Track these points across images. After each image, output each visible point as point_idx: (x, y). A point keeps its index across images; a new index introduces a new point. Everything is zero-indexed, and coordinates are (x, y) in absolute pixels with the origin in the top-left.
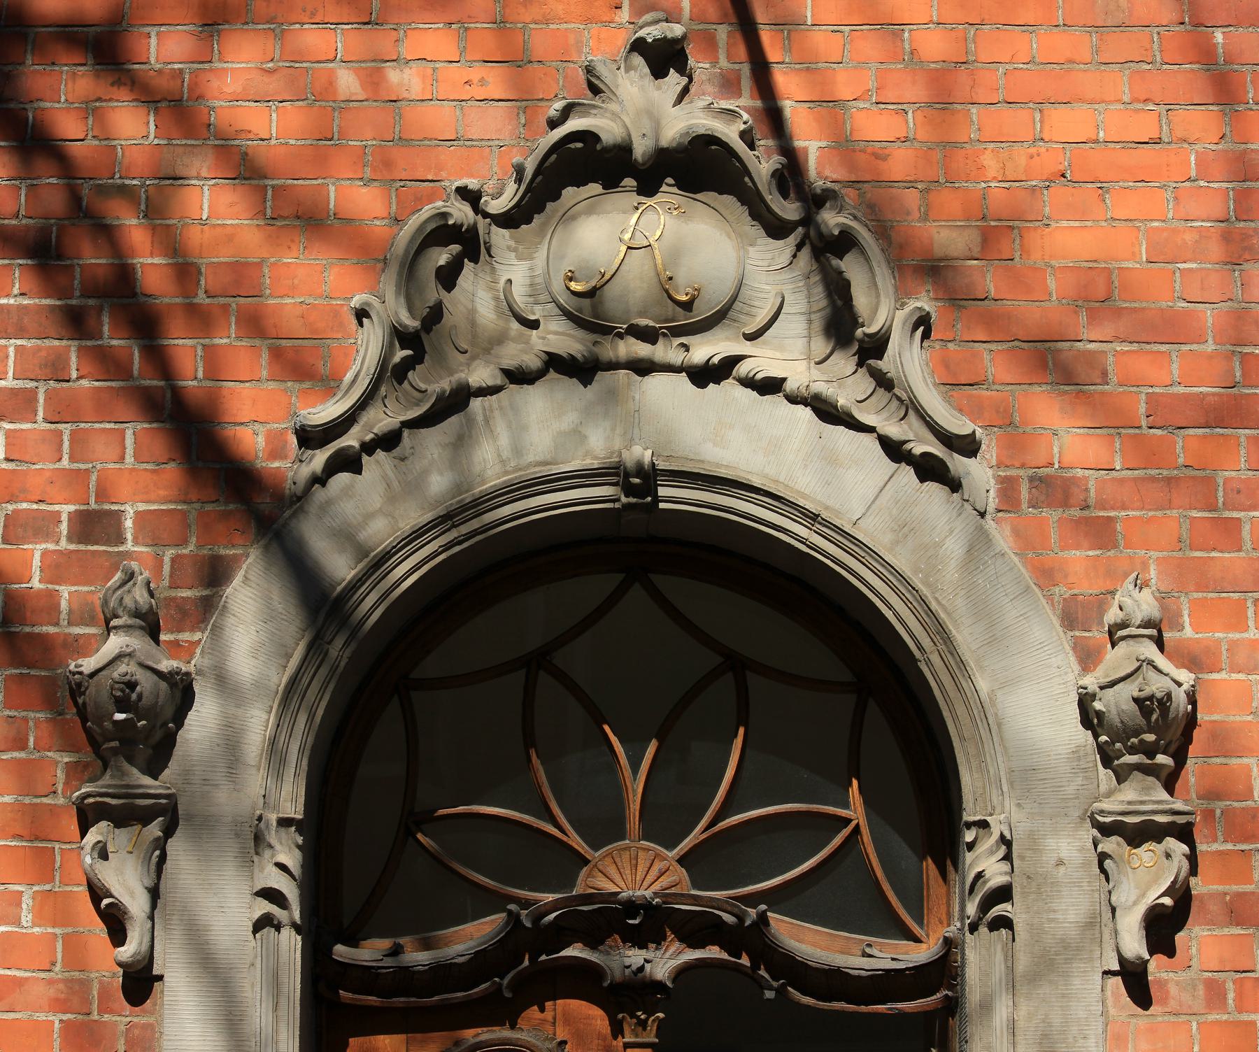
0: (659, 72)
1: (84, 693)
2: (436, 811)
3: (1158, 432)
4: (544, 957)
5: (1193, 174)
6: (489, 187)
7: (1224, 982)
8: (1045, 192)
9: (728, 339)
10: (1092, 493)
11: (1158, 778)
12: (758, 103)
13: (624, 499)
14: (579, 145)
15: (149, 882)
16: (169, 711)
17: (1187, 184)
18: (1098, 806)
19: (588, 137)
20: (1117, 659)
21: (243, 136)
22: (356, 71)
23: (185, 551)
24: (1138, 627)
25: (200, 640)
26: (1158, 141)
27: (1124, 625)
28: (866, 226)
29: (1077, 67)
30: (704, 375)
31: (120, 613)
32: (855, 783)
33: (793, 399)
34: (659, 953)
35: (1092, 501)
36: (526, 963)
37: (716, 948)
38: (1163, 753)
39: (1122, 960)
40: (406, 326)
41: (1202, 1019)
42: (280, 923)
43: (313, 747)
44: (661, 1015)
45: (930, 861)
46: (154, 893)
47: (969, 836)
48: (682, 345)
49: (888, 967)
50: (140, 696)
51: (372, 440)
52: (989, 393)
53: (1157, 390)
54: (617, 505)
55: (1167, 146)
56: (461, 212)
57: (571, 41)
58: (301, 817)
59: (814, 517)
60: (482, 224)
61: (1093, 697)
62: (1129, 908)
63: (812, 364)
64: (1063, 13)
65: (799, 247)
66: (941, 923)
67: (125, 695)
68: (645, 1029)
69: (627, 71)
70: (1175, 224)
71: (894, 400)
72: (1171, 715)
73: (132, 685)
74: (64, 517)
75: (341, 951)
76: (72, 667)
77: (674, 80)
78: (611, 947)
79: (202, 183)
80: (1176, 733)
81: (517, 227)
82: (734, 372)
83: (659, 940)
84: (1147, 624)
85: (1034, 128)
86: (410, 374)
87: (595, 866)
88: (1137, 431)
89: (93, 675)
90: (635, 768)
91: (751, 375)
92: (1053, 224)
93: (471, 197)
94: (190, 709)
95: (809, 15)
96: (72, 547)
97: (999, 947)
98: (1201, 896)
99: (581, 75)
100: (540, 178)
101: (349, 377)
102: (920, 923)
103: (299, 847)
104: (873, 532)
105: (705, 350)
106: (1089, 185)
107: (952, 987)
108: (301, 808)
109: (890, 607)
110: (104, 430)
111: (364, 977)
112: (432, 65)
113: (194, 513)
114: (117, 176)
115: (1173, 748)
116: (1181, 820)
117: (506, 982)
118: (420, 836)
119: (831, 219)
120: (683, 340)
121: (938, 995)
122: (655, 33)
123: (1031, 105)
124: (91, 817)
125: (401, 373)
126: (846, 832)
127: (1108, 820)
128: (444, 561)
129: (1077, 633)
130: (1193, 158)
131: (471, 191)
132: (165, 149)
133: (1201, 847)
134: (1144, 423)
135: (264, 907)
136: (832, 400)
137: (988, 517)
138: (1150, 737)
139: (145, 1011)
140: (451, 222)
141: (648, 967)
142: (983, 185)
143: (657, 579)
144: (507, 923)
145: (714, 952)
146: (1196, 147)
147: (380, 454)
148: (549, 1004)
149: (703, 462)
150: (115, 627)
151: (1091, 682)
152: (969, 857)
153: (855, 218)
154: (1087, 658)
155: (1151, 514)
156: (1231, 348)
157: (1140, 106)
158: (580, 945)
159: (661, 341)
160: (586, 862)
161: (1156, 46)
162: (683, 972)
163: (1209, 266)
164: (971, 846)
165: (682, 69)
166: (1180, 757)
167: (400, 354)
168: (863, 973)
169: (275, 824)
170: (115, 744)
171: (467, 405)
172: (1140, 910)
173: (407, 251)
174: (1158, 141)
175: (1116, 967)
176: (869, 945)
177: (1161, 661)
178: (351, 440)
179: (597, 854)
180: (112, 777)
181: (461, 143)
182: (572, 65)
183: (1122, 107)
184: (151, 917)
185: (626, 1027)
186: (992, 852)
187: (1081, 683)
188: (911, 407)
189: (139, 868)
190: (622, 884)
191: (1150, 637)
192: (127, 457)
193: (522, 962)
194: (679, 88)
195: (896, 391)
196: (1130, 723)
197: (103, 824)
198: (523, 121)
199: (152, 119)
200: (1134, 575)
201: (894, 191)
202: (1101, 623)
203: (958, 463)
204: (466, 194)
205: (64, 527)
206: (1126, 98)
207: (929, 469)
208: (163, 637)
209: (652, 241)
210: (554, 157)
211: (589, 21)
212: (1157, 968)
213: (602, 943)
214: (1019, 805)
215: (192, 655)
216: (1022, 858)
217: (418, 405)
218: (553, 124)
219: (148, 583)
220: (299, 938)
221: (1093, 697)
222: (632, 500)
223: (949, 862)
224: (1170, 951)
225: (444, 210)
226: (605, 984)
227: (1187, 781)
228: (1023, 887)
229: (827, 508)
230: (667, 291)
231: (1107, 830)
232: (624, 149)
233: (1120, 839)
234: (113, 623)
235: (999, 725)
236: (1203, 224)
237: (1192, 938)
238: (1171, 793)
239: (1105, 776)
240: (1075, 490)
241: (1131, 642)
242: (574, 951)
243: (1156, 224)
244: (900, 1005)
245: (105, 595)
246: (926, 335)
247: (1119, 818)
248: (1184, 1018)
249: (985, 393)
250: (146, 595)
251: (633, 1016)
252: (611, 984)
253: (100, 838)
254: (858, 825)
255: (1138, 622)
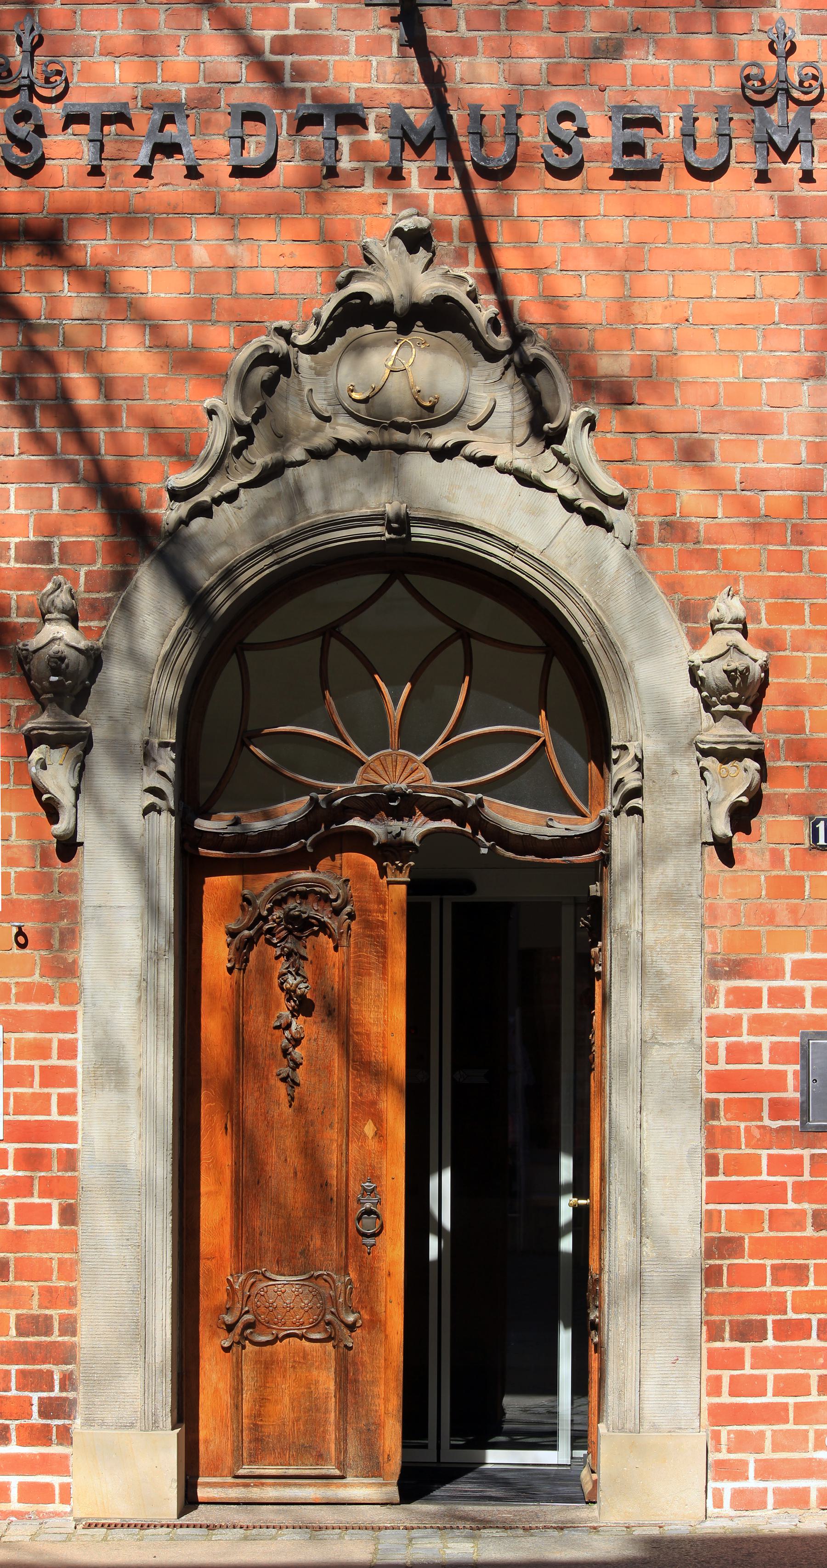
0: (412, 249)
1: (29, 663)
2: (263, 730)
3: (748, 493)
4: (334, 826)
5: (777, 319)
6: (298, 325)
7: (783, 850)
8: (675, 332)
9: (458, 430)
10: (702, 534)
11: (740, 720)
12: (482, 270)
13: (387, 536)
14: (358, 301)
15: (74, 783)
16: (85, 674)
17: (772, 326)
18: (700, 737)
19: (364, 296)
20: (716, 644)
21: (129, 290)
22: (206, 246)
23: (95, 568)
24: (730, 623)
25: (105, 627)
26: (753, 297)
27: (720, 621)
28: (552, 354)
29: (699, 246)
30: (442, 454)
31: (52, 610)
32: (543, 713)
33: (502, 470)
34: (411, 824)
35: (701, 539)
36: (323, 829)
37: (449, 821)
38: (744, 704)
39: (714, 836)
40: (241, 421)
41: (768, 874)
42: (160, 808)
43: (182, 696)
44: (412, 863)
45: (593, 764)
46: (77, 790)
47: (615, 755)
48: (427, 434)
49: (562, 834)
50: (67, 666)
51: (220, 496)
52: (634, 467)
53: (748, 465)
54: (383, 538)
55: (759, 301)
56: (278, 345)
57: (353, 226)
58: (174, 741)
59: (515, 548)
60: (293, 351)
61: (698, 667)
62: (720, 803)
63: (514, 446)
64: (691, 209)
65: (506, 368)
66: (600, 805)
67: (57, 663)
68: (401, 872)
69: (390, 249)
70: (763, 353)
71: (569, 471)
72: (749, 681)
73: (62, 659)
74: (13, 546)
75: (203, 825)
76: (20, 645)
77: (423, 255)
78: (378, 820)
79: (101, 323)
80: (753, 692)
81: (316, 353)
82: (462, 452)
83: (411, 815)
84: (735, 621)
85: (668, 288)
86: (244, 452)
87: (369, 766)
88: (734, 493)
89: (35, 651)
90: (395, 702)
91: (473, 454)
92: (680, 354)
93: (285, 334)
94: (100, 671)
95: (515, 209)
96: (18, 565)
97: (633, 826)
98: (769, 795)
99: (360, 251)
100: (331, 322)
101: (203, 453)
102: (586, 804)
103: (173, 760)
104: (557, 559)
105: (442, 438)
106: (705, 327)
107: (605, 848)
108: (174, 735)
109: (565, 606)
110: (38, 488)
111: (214, 840)
112: (257, 243)
113: (100, 543)
114: (43, 317)
115: (751, 701)
116: (754, 748)
117: (309, 842)
118: (252, 747)
119: (531, 350)
120: (428, 431)
121: (596, 853)
122: (410, 225)
123: (666, 272)
124: (34, 742)
125: (238, 451)
126: (537, 744)
127: (706, 746)
128: (268, 574)
129: (689, 625)
130: (777, 309)
131: (284, 330)
132: (76, 299)
133: (769, 764)
134: (738, 488)
135: (151, 799)
136: (528, 472)
137: (631, 548)
138: (735, 695)
139: (71, 866)
140: (271, 352)
141: (403, 832)
142: (632, 326)
143: (409, 577)
144: (310, 805)
145: (447, 823)
146: (780, 301)
147: (225, 505)
148: (337, 856)
149: (440, 512)
150: (49, 620)
151: (698, 657)
152: (615, 768)
153: (544, 348)
154: (697, 640)
155: (741, 547)
156: (800, 438)
157: (741, 273)
158: (358, 818)
159: (412, 432)
160: (363, 763)
161: (754, 231)
162: (426, 837)
163: (786, 380)
164: (616, 761)
165: (429, 248)
166: (757, 706)
167: (237, 440)
168: (547, 838)
169: (157, 745)
170: (49, 696)
171: (283, 473)
172: (727, 804)
173: (241, 370)
174: (753, 297)
175: (711, 840)
176: (551, 820)
177: (744, 645)
178: (204, 497)
179: (370, 758)
180: (49, 716)
181: (278, 296)
182: (353, 244)
183: (729, 273)
184: (76, 806)
185: (388, 870)
186: (629, 766)
187: (690, 658)
188: (581, 477)
189: (67, 774)
190: (387, 778)
191: (737, 629)
192: (54, 506)
193: (320, 829)
194: (426, 260)
195: (571, 465)
196: (722, 686)
197: (43, 747)
198: (320, 282)
199: (66, 279)
200: (727, 589)
201: (571, 330)
202: (706, 618)
203: (611, 514)
204: (285, 334)
205: (12, 553)
206: (732, 268)
207: (592, 518)
208: (80, 624)
209: (406, 366)
210: (340, 310)
211: (364, 213)
212: (739, 842)
213: (373, 817)
214: (648, 735)
215: (100, 635)
216: (649, 769)
217: (249, 473)
218: (341, 286)
219: (70, 590)
220: (173, 818)
221: (698, 667)
222: (392, 536)
223: (605, 766)
224: (748, 831)
225: (266, 343)
226: (375, 844)
227: (761, 721)
228: (650, 788)
229: (523, 542)
230: (416, 400)
231: (705, 753)
232: (387, 305)
233: (714, 759)
234: (47, 617)
235: (636, 684)
236: (783, 354)
237: (761, 822)
238: (750, 729)
239: (706, 717)
240: (690, 531)
241: (724, 632)
242: (356, 822)
243: (749, 354)
244: (571, 859)
245: (42, 597)
246: (592, 429)
247: (714, 746)
248: (755, 873)
249: (631, 466)
250: (69, 598)
251: (393, 864)
252: (379, 844)
253: (41, 756)
254: (544, 741)
255: (729, 620)
